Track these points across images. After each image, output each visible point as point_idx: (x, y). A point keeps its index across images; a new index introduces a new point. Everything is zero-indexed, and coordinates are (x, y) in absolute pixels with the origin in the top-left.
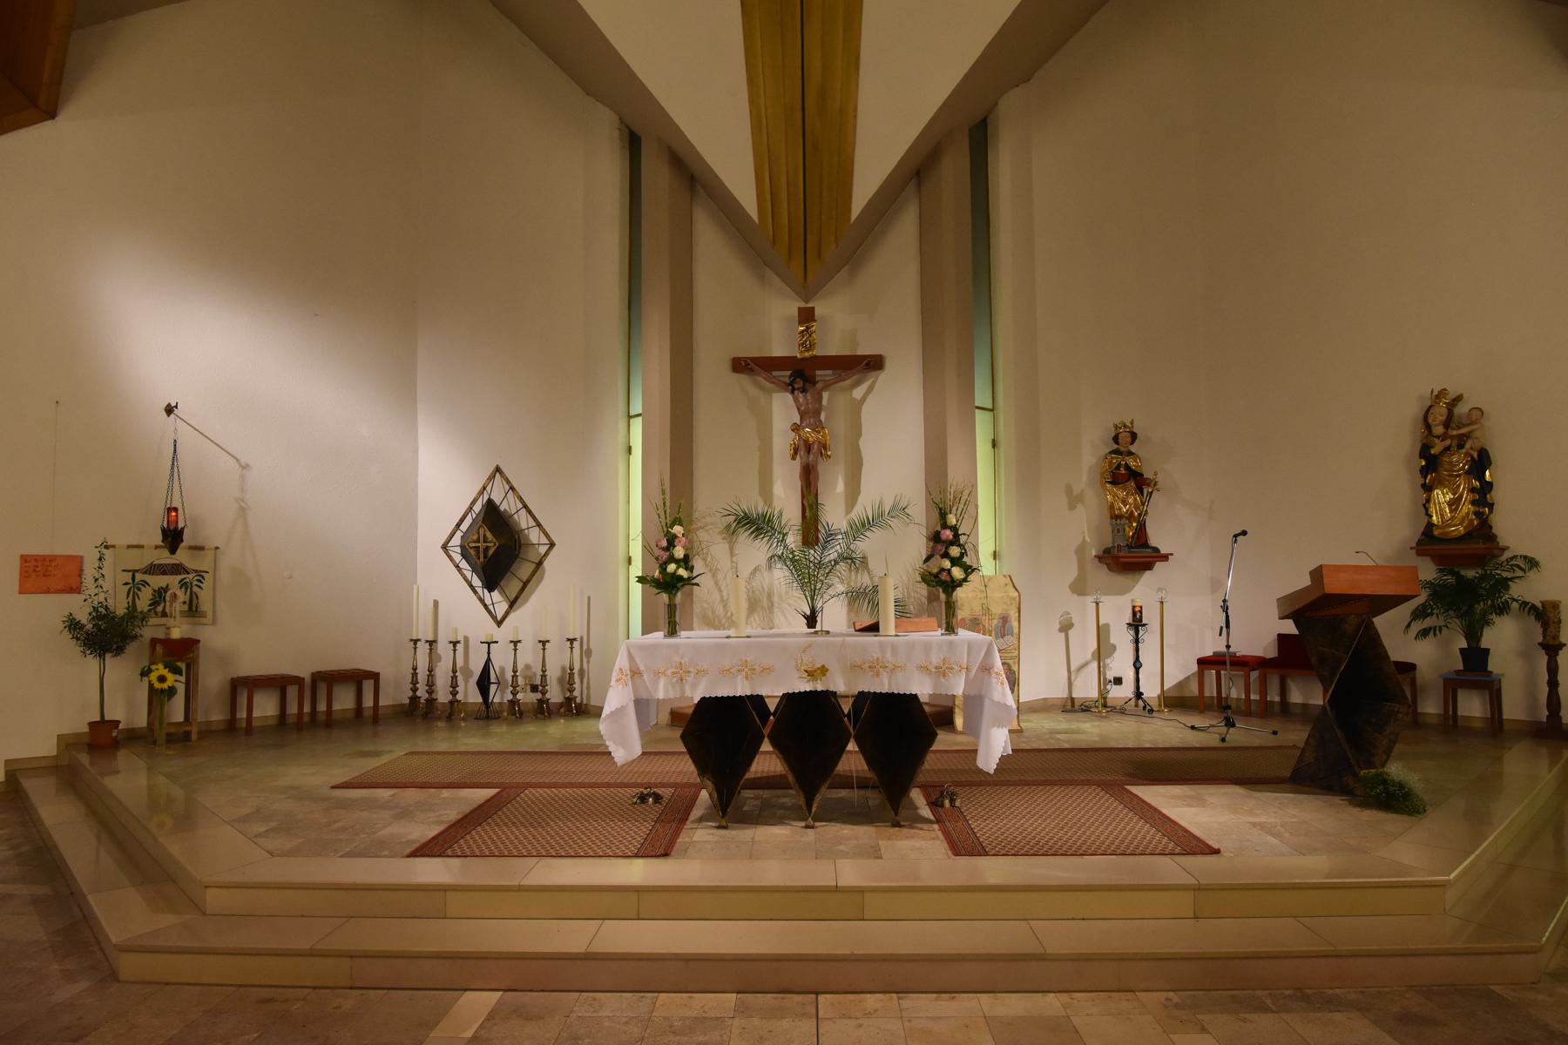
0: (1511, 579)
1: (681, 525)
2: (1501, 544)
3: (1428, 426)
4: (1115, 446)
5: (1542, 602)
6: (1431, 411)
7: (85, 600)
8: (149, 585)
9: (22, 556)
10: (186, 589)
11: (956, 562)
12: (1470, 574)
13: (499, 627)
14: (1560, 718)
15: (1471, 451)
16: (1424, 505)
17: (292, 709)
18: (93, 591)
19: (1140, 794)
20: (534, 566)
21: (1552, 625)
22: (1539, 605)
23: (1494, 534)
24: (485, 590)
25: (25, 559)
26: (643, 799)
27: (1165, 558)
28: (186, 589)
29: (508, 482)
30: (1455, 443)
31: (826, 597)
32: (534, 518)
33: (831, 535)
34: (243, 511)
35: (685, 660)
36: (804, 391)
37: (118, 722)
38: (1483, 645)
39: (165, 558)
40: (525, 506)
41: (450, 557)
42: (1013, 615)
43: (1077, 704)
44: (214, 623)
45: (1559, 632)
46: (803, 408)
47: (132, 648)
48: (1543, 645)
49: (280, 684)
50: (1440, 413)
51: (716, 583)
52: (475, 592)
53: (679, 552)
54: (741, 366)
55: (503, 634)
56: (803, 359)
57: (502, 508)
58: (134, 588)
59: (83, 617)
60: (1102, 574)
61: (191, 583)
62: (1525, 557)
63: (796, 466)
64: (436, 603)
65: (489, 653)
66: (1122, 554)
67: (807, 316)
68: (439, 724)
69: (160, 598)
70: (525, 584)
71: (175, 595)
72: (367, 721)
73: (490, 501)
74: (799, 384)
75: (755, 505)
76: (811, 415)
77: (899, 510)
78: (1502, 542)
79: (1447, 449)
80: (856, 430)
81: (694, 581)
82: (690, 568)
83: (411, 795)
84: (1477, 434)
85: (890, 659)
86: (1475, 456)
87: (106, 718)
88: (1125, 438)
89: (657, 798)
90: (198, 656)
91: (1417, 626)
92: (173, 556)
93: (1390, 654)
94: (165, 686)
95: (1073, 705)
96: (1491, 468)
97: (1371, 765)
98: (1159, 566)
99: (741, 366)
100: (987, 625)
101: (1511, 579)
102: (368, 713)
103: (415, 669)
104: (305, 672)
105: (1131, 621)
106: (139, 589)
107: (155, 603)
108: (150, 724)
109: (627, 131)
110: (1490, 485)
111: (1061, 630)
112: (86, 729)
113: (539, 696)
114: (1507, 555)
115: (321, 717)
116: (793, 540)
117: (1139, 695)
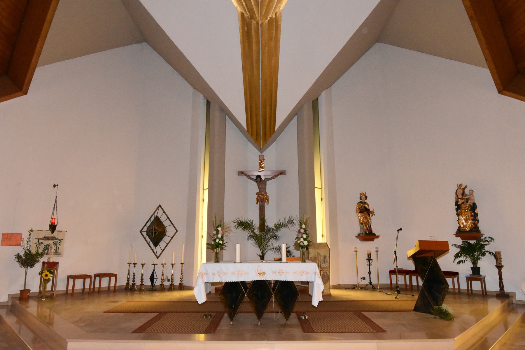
0: (486, 245)
1: (221, 227)
2: (482, 233)
3: (457, 195)
4: (361, 201)
5: (495, 252)
6: (457, 191)
7: (23, 249)
8: (43, 244)
9: (3, 233)
10: (55, 245)
11: (305, 239)
12: (472, 242)
13: (158, 259)
14: (504, 290)
15: (470, 204)
16: (458, 220)
18: (26, 246)
19: (368, 316)
20: (145, 237)
21: (499, 260)
22: (495, 253)
23: (479, 230)
24: (154, 247)
27: (378, 237)
28: (55, 245)
30: (465, 200)
31: (267, 250)
33: (269, 230)
38: (478, 266)
39: (49, 234)
45: (501, 262)
48: (497, 266)
50: (460, 191)
52: (150, 247)
55: (159, 261)
58: (38, 244)
59: (22, 254)
61: (57, 243)
62: (490, 237)
65: (154, 268)
69: (46, 248)
73: (157, 216)
77: (291, 222)
78: (482, 232)
79: (463, 203)
81: (225, 245)
82: (223, 241)
86: (472, 205)
87: (26, 289)
88: (363, 197)
90: (58, 268)
91: (458, 260)
92: (52, 234)
93: (441, 269)
94: (47, 278)
97: (437, 305)
98: (376, 240)
100: (319, 259)
101: (486, 245)
105: (367, 258)
106: (40, 245)
107: (44, 250)
109: (206, 100)
112: (19, 292)
113: (170, 283)
114: (484, 236)
116: (257, 231)
117: (371, 283)
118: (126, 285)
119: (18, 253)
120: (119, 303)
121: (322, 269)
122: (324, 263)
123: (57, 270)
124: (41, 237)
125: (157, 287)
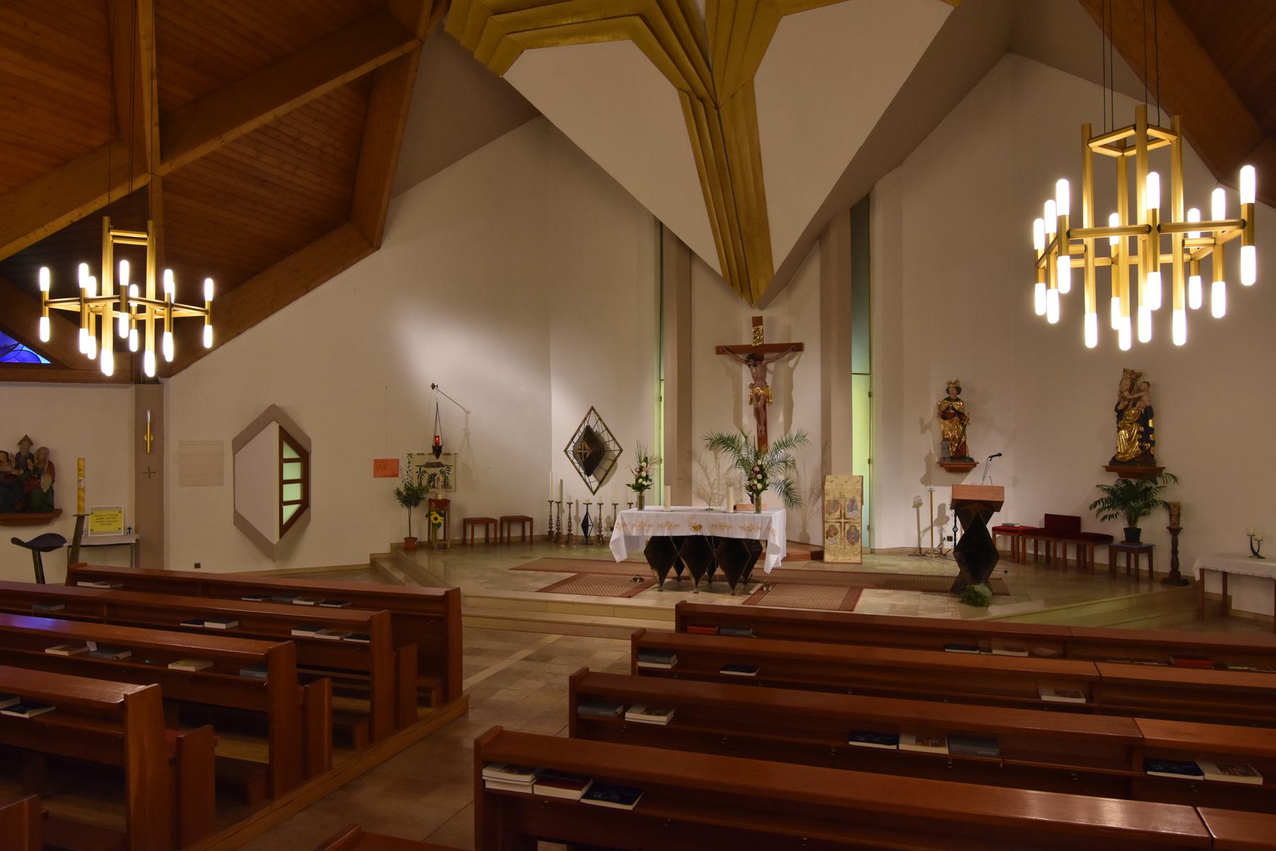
11: (759, 481)
17: (492, 535)
18: (406, 477)
20: (611, 462)
25: (376, 461)
26: (635, 580)
29: (598, 415)
32: (611, 435)
34: (467, 435)
35: (644, 520)
36: (755, 365)
37: (416, 538)
38: (1138, 527)
39: (433, 459)
40: (607, 429)
41: (568, 456)
42: (858, 499)
43: (923, 552)
44: (455, 491)
46: (755, 375)
47: (422, 503)
49: (485, 522)
51: (706, 475)
52: (581, 475)
53: (644, 474)
54: (721, 350)
56: (756, 347)
57: (594, 430)
58: (421, 474)
59: (402, 489)
60: (942, 473)
63: (752, 408)
64: (562, 481)
65: (587, 509)
66: (945, 463)
67: (757, 321)
68: (563, 546)
70: (607, 472)
71: (439, 478)
72: (527, 542)
74: (752, 361)
75: (730, 431)
76: (759, 379)
79: (1127, 406)
80: (790, 387)
83: (541, 574)
84: (1145, 398)
85: (728, 522)
87: (412, 536)
88: (953, 390)
89: (641, 580)
94: (437, 522)
95: (920, 552)
96: (1154, 418)
99: (721, 350)
102: (528, 539)
103: (551, 517)
104: (497, 517)
107: (429, 482)
108: (429, 539)
110: (1152, 430)
111: (914, 507)
112: (404, 541)
115: (505, 540)
118: (549, 535)
119: (398, 489)
120: (534, 559)
121: (847, 521)
122: (852, 511)
123: (449, 510)
124: (424, 462)
125: (593, 539)
